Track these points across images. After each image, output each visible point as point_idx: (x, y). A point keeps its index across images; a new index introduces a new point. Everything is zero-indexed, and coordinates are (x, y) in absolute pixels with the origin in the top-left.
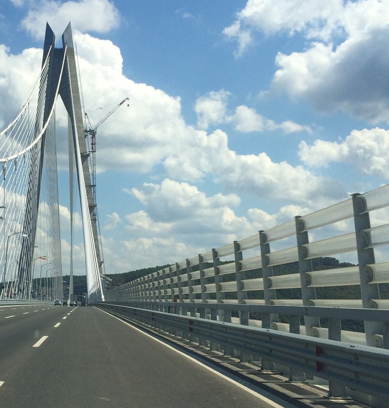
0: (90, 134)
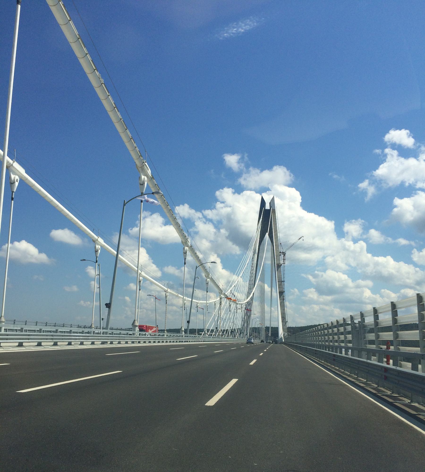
0: (283, 254)
